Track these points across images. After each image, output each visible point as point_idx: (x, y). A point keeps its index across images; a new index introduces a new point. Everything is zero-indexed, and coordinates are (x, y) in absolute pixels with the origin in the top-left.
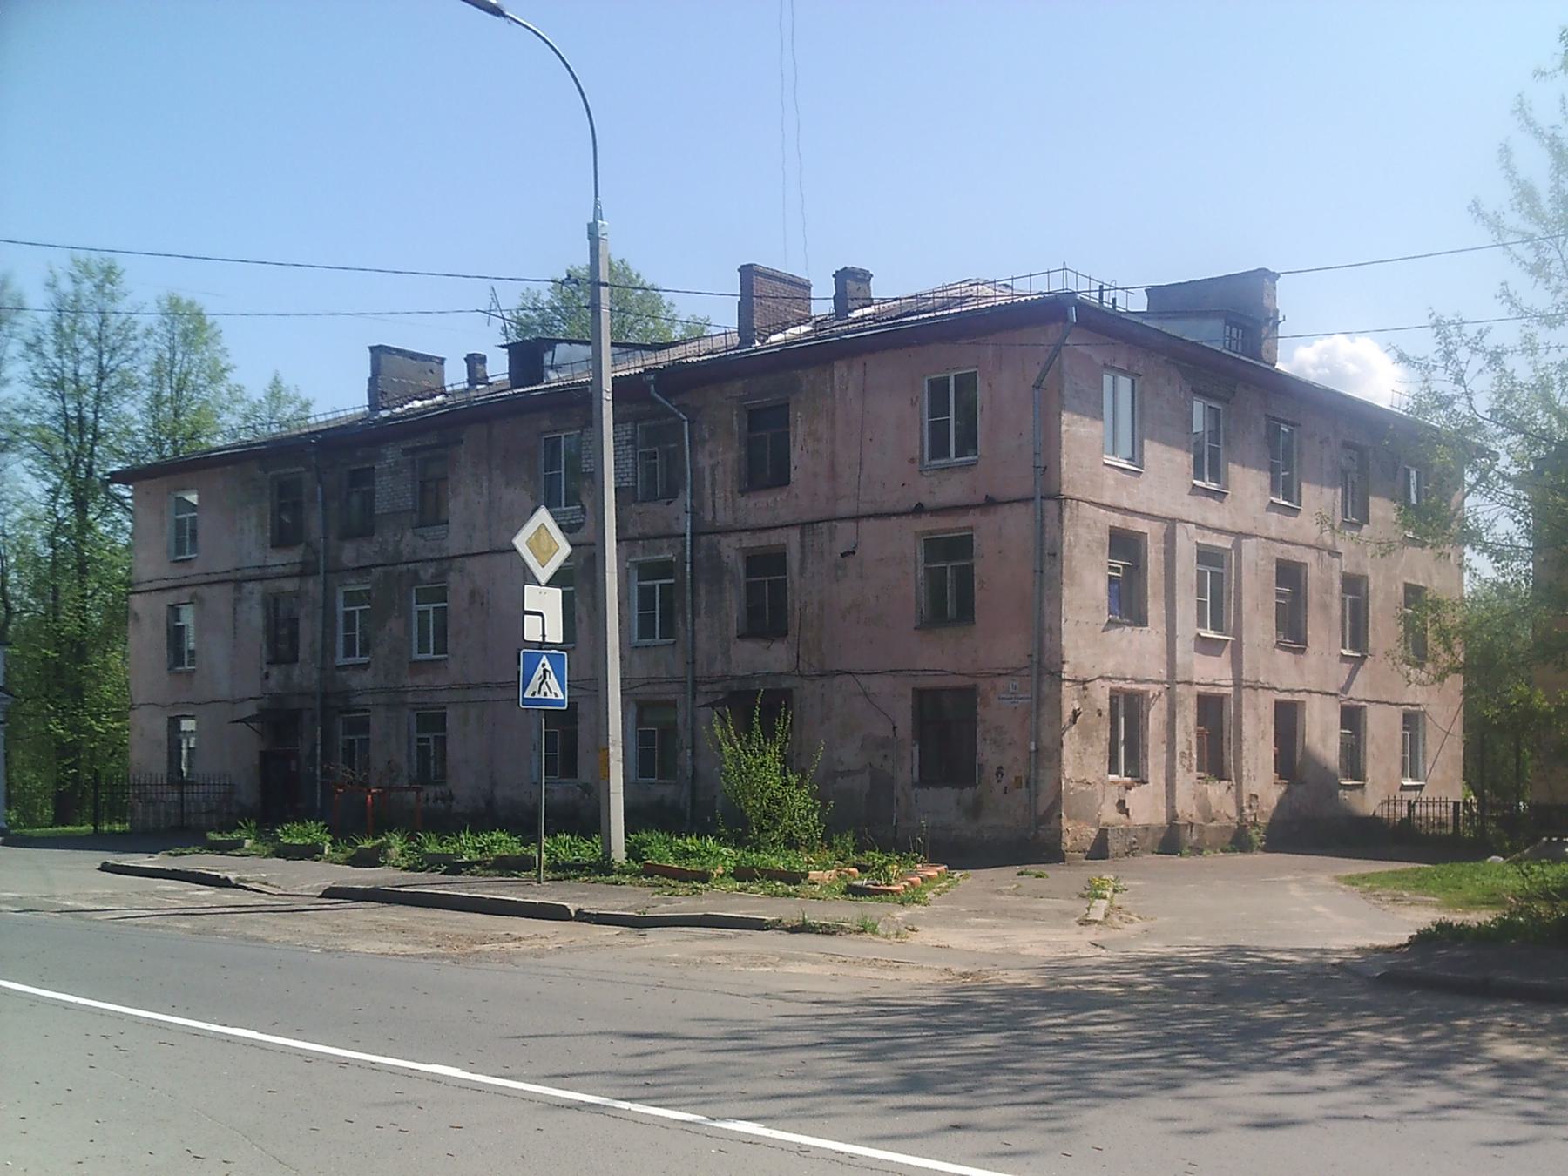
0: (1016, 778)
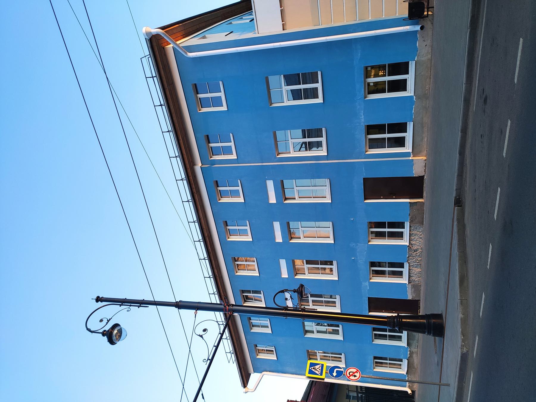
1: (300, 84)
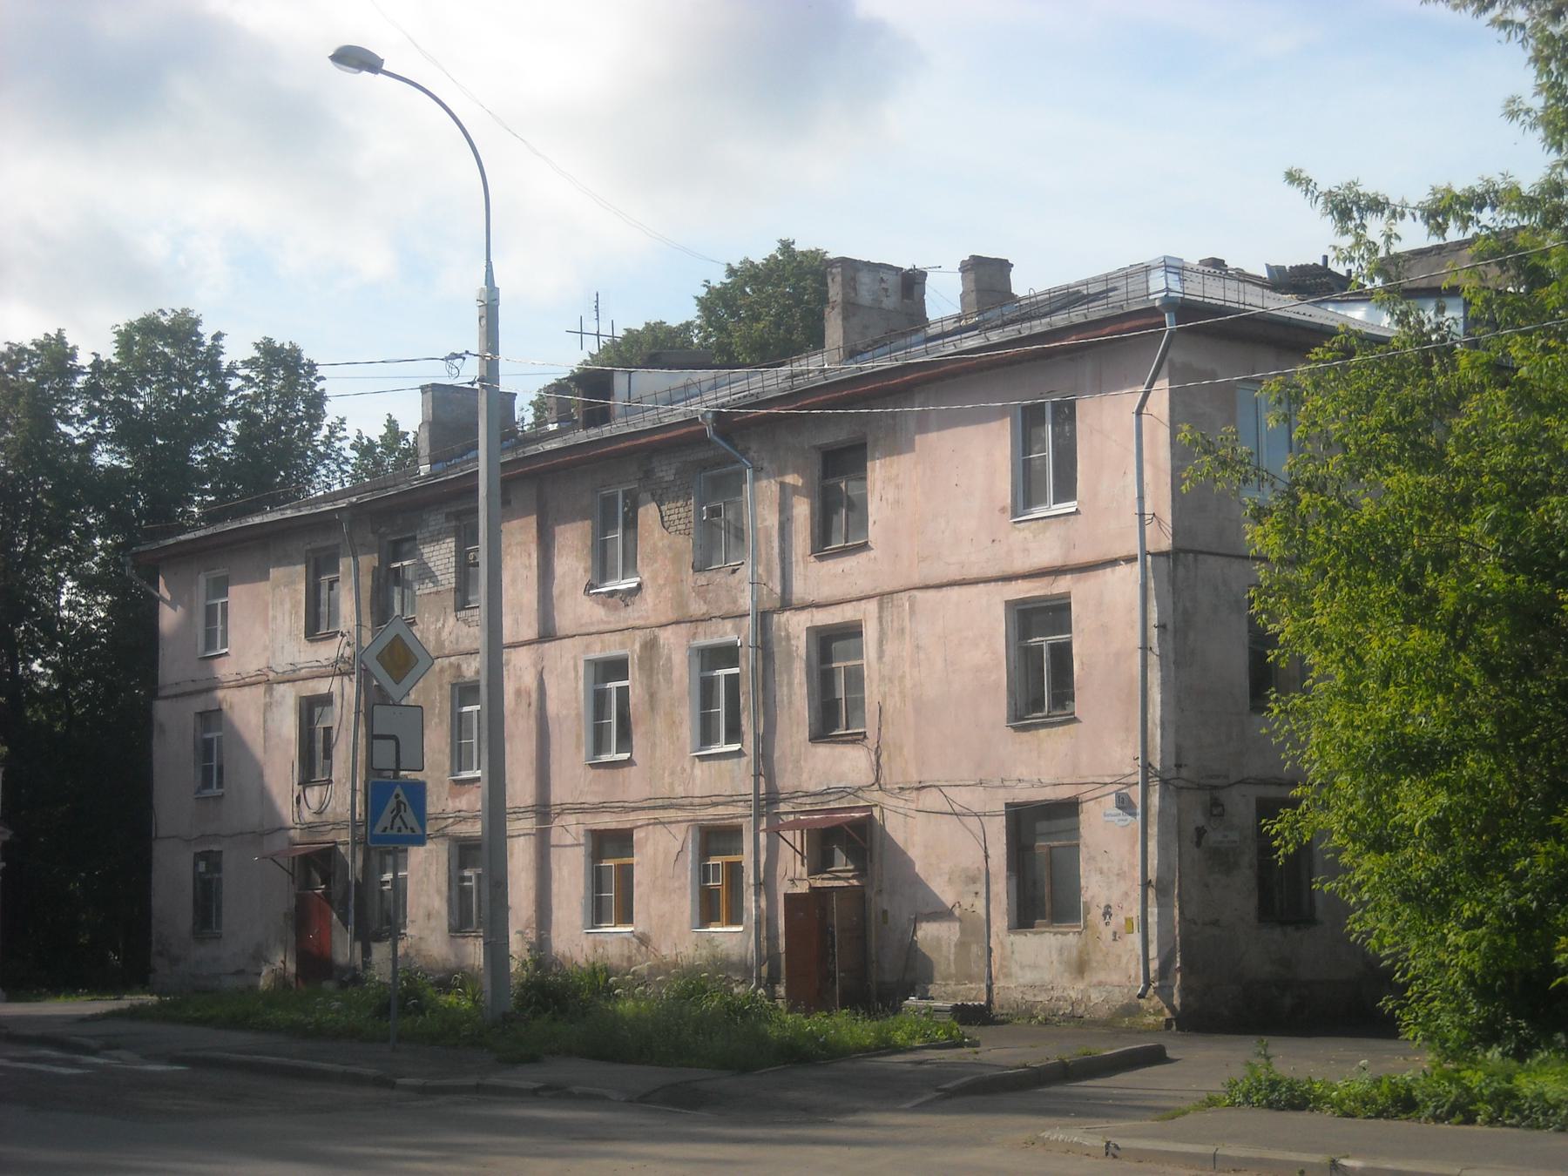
0: (1126, 919)
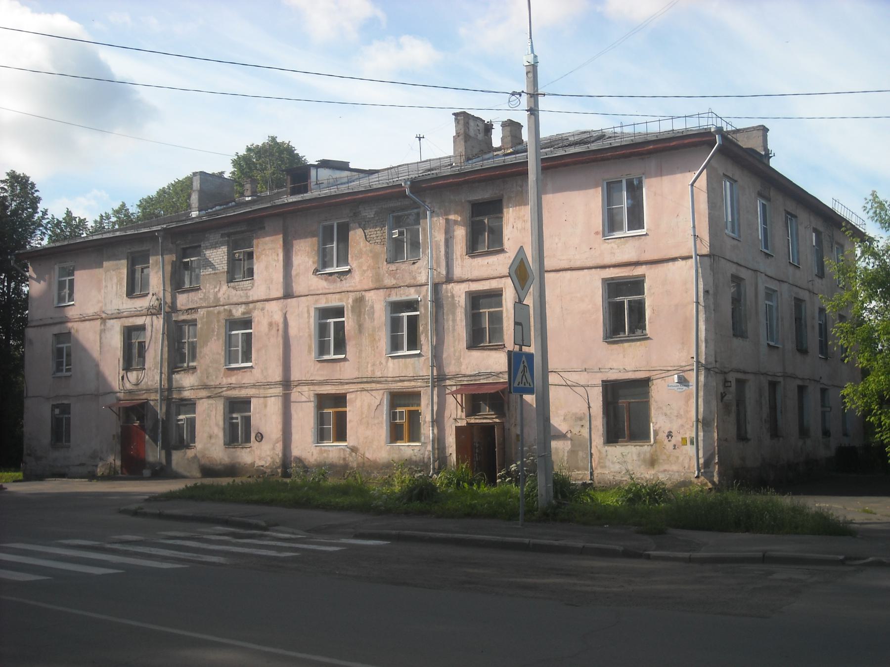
0: (682, 439)
1: (63, 361)
